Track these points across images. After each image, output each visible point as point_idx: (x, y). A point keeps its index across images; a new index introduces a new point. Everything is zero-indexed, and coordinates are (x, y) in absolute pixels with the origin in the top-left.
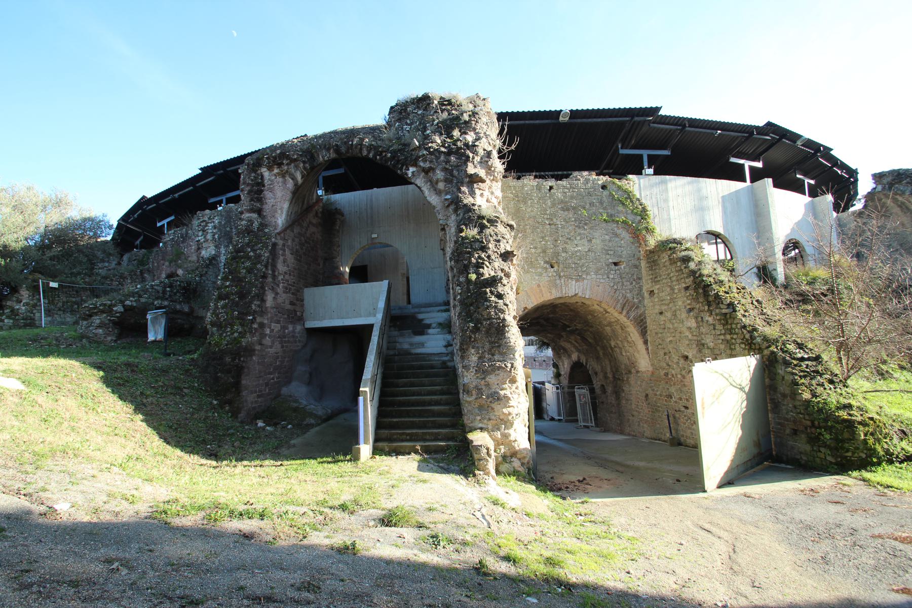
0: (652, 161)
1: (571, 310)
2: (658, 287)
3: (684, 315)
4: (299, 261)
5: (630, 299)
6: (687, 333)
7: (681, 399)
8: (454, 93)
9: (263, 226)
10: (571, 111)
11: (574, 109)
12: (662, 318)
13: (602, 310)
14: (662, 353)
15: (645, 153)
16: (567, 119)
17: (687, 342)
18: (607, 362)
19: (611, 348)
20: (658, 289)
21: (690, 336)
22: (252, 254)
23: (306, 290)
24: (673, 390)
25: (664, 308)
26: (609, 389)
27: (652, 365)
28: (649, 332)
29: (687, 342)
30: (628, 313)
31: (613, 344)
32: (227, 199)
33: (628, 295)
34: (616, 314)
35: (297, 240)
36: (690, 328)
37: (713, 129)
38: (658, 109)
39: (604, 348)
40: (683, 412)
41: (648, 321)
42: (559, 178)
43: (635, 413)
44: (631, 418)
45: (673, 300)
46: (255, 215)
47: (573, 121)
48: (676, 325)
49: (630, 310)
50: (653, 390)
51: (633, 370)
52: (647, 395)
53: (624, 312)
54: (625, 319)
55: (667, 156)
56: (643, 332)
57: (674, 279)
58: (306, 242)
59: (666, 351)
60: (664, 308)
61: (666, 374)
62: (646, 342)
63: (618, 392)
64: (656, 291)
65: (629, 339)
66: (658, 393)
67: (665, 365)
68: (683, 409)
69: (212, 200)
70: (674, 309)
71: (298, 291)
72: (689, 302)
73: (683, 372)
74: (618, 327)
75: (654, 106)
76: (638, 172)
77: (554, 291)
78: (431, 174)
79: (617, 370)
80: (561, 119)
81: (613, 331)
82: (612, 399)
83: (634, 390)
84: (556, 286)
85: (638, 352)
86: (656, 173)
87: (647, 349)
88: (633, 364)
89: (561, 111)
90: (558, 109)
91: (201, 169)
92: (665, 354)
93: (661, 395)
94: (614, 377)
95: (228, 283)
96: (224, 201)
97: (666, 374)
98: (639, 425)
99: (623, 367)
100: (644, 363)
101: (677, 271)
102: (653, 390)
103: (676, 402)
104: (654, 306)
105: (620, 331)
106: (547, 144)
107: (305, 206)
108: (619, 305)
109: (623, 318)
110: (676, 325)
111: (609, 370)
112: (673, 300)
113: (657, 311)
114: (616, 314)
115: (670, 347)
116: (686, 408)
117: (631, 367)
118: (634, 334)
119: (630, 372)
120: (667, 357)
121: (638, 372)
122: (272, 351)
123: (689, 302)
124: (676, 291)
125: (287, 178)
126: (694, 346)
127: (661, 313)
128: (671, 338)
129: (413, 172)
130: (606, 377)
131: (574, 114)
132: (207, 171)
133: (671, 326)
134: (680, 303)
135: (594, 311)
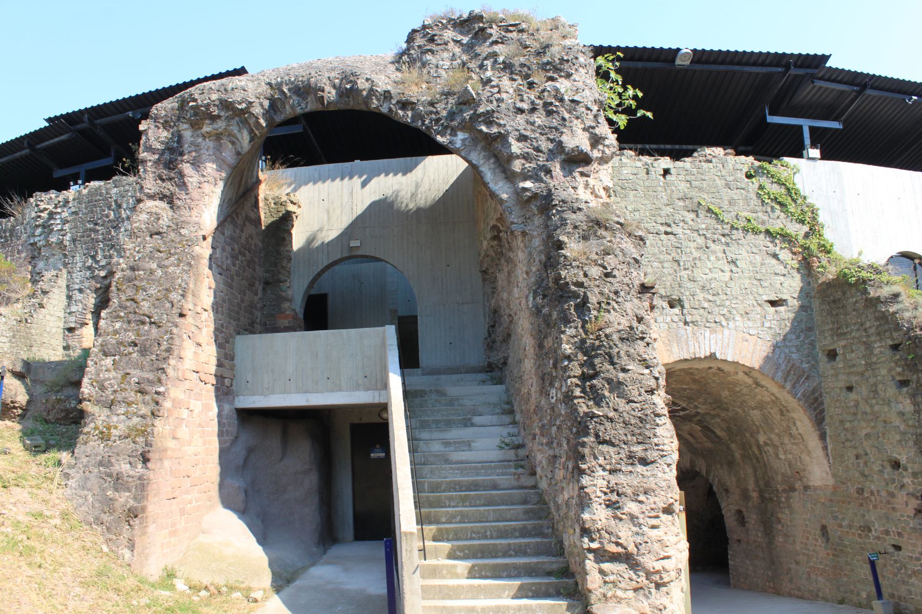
0: (818, 137)
1: (695, 381)
2: (843, 343)
3: (891, 391)
4: (231, 286)
5: (798, 364)
6: (897, 422)
7: (887, 533)
8: (523, 11)
9: (177, 226)
10: (695, 51)
11: (699, 48)
12: (853, 396)
13: (749, 381)
14: (851, 454)
15: (806, 124)
16: (688, 63)
17: (898, 437)
18: (750, 471)
19: (759, 446)
20: (844, 347)
21: (902, 427)
22: (159, 272)
23: (238, 337)
24: (872, 517)
25: (854, 379)
26: (752, 518)
27: (834, 475)
28: (827, 420)
29: (898, 437)
30: (794, 386)
31: (762, 439)
32: (87, 171)
33: (794, 356)
34: (775, 389)
35: (228, 248)
36: (901, 414)
37: (905, 93)
38: (825, 58)
39: (745, 446)
40: (892, 555)
41: (827, 400)
42: (677, 156)
43: (801, 558)
44: (793, 566)
45: (870, 366)
46: (163, 205)
47: (698, 67)
48: (876, 408)
49: (797, 381)
50: (836, 518)
51: (798, 485)
52: (824, 528)
53: (788, 386)
54: (790, 398)
55: (837, 130)
56: (819, 420)
57: (873, 330)
58: (240, 253)
59: (861, 452)
60: (854, 379)
61: (860, 491)
62: (823, 437)
63: (768, 524)
64: (840, 351)
65: (794, 432)
66: (844, 523)
67: (857, 474)
68: (891, 550)
69: (58, 173)
70: (872, 380)
71: (227, 342)
72: (899, 370)
73: (891, 488)
74: (774, 412)
75: (820, 53)
76: (797, 152)
77: (675, 349)
78: (497, 145)
79: (767, 484)
80: (678, 62)
81: (765, 418)
82: (755, 533)
83: (800, 522)
84: (678, 339)
85: (809, 453)
86: (823, 157)
87: (825, 448)
88: (799, 474)
89: (679, 50)
90: (674, 47)
91: (49, 120)
92: (857, 457)
93: (850, 526)
94: (762, 497)
95: (118, 325)
96: (83, 174)
97: (860, 491)
98: (809, 578)
99: (779, 478)
100: (819, 472)
101: (877, 319)
102: (836, 518)
103: (878, 538)
104: (836, 375)
105: (778, 417)
106: (695, 103)
107: (242, 190)
108: (780, 374)
109: (785, 397)
110: (876, 408)
111: (751, 485)
112: (871, 366)
113: (842, 384)
114: (775, 389)
115: (867, 444)
116: (898, 548)
117: (795, 480)
118: (803, 423)
119: (793, 489)
120: (861, 461)
121: (806, 488)
122: (190, 450)
123: (899, 370)
124: (876, 351)
125: (225, 141)
126: (911, 443)
127: (850, 389)
128: (868, 430)
129: (463, 140)
130: (745, 496)
131: (700, 56)
132: (58, 124)
133: (868, 410)
134: (884, 372)
135: (736, 383)
